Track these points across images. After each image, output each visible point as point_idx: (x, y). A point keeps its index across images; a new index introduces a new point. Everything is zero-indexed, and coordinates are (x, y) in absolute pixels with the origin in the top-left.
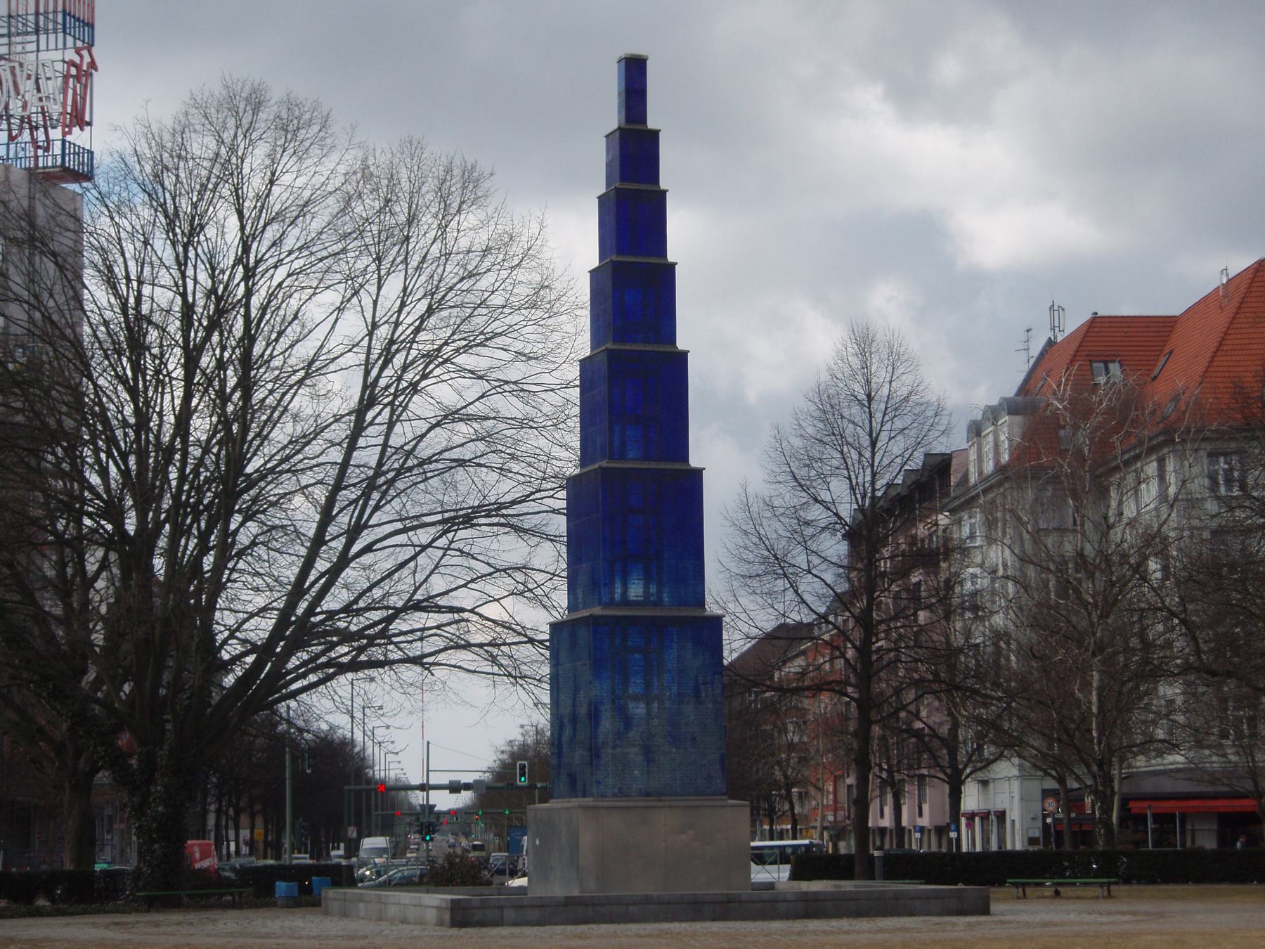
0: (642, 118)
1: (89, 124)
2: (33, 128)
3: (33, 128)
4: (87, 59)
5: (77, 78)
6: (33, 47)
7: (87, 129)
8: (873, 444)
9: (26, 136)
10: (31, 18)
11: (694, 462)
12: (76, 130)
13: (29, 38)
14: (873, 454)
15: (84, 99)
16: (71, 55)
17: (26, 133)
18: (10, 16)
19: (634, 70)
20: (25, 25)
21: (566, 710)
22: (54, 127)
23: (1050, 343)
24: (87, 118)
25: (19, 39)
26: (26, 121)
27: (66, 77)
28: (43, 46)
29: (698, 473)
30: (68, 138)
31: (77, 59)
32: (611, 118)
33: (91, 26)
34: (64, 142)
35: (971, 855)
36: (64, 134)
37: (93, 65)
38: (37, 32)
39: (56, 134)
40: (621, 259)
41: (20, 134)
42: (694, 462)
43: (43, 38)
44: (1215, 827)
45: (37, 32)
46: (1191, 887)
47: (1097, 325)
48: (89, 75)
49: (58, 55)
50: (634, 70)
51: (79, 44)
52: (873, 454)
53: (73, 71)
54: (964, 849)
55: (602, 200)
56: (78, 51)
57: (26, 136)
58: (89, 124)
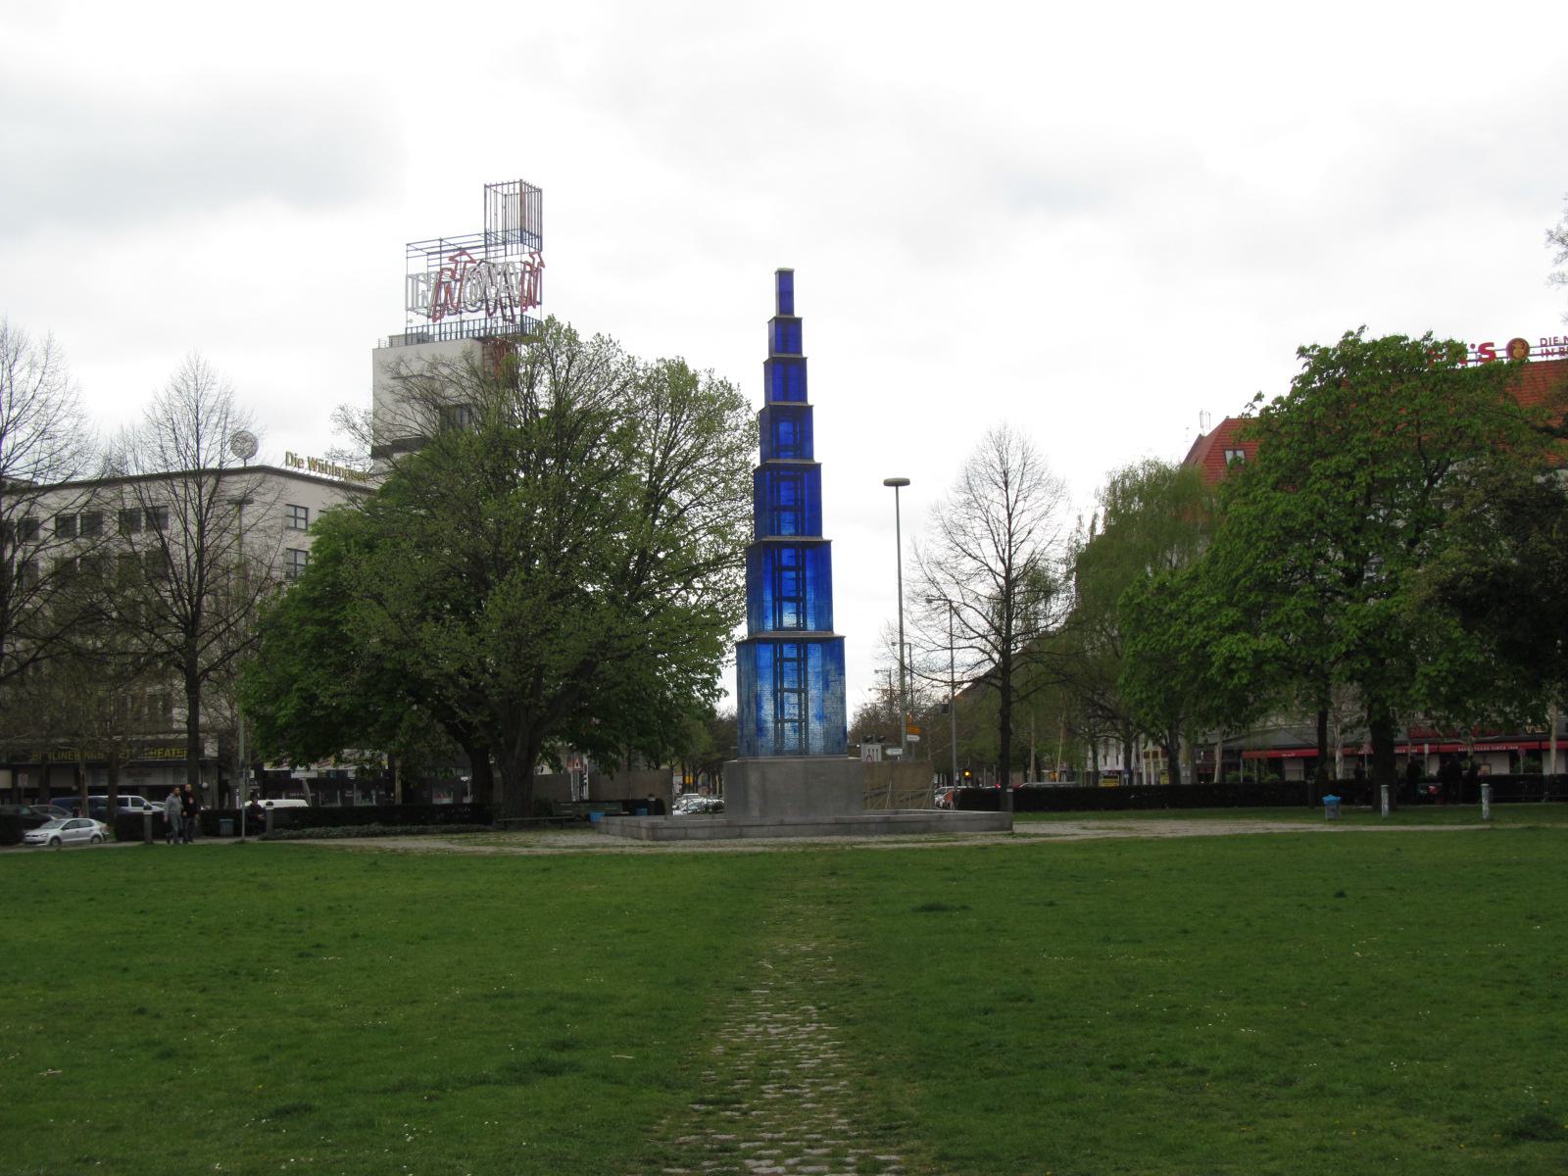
0: (791, 311)
1: (540, 303)
2: (503, 308)
3: (503, 308)
4: (538, 260)
5: (530, 272)
6: (502, 253)
7: (538, 307)
8: (1010, 516)
9: (499, 313)
10: (500, 234)
11: (826, 536)
12: (530, 308)
13: (499, 247)
14: (1010, 523)
15: (535, 287)
16: (527, 258)
17: (499, 310)
18: (486, 234)
19: (785, 279)
20: (496, 239)
21: (744, 698)
22: (517, 306)
23: (1201, 438)
24: (538, 299)
25: (492, 248)
26: (498, 302)
27: (523, 272)
28: (509, 252)
29: (828, 544)
30: (525, 313)
31: (531, 261)
32: (771, 310)
33: (540, 238)
34: (522, 316)
35: (1149, 787)
36: (522, 311)
37: (541, 264)
38: (504, 243)
39: (517, 311)
40: (776, 403)
41: (495, 311)
42: (826, 536)
43: (509, 247)
44: (1302, 768)
45: (504, 243)
46: (1148, 812)
47: (1228, 424)
48: (538, 270)
49: (516, 259)
50: (785, 279)
51: (532, 250)
52: (1010, 523)
53: (528, 268)
54: (1145, 783)
55: (766, 363)
56: (531, 255)
57: (499, 313)
58: (540, 303)
